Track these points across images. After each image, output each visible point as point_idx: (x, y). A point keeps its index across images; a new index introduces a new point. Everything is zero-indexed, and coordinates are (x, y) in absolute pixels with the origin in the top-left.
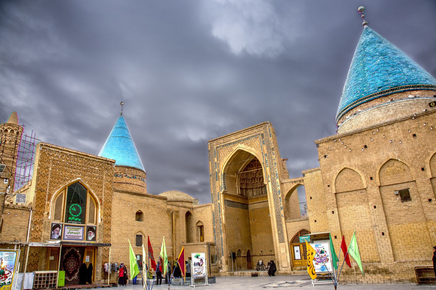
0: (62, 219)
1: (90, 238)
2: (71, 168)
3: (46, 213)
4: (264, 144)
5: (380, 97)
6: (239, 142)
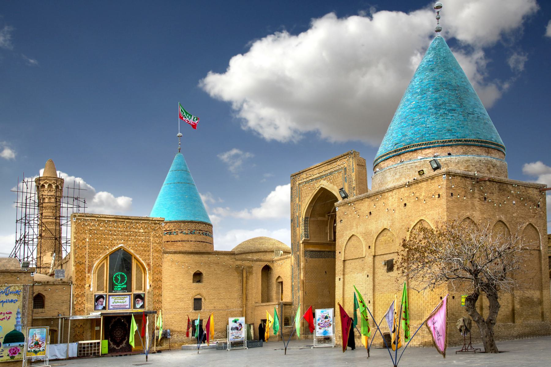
0: (105, 290)
1: (138, 306)
2: (111, 235)
3: (87, 285)
4: (346, 181)
5: (394, 156)
6: (321, 177)
